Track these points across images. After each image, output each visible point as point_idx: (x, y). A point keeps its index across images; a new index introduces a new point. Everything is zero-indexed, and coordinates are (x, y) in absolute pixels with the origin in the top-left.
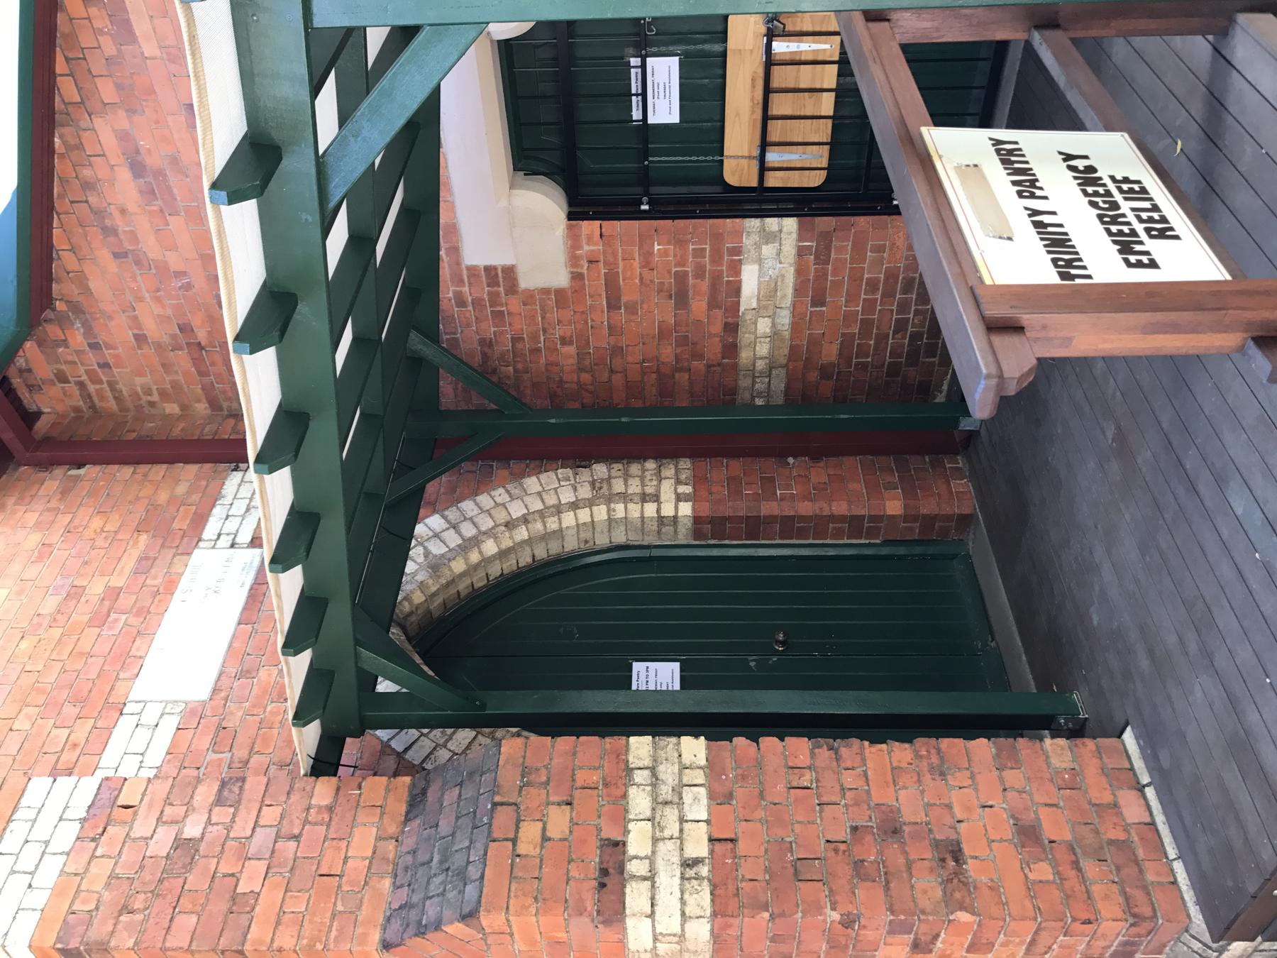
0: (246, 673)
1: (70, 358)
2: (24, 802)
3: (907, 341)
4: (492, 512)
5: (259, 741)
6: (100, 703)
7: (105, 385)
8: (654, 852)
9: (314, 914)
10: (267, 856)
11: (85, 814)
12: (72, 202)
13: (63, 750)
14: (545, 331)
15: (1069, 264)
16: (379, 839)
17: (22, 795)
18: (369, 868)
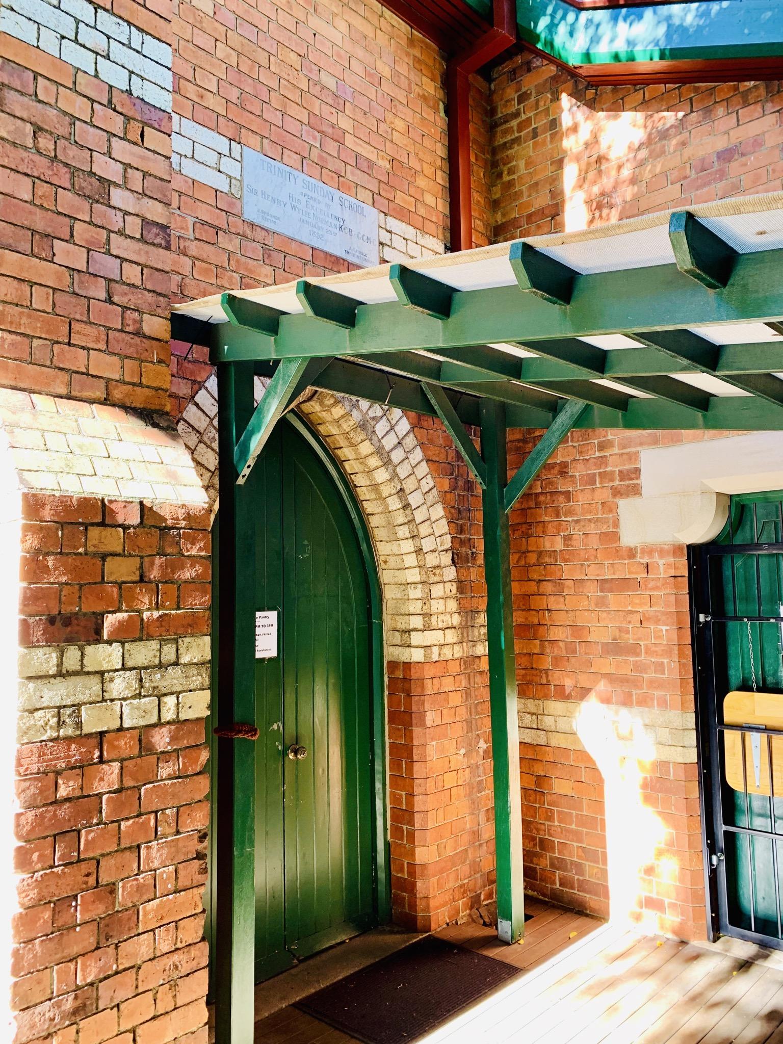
0: (267, 250)
1: (542, 103)
2: (148, 38)
3: (575, 859)
5: (205, 265)
6: (237, 124)
7: (517, 135)
8: (88, 673)
9: (29, 316)
10: (90, 270)
11: (135, 95)
12: (691, 99)
13: (197, 85)
14: (577, 521)
16: (108, 381)
17: (155, 37)
18: (77, 372)
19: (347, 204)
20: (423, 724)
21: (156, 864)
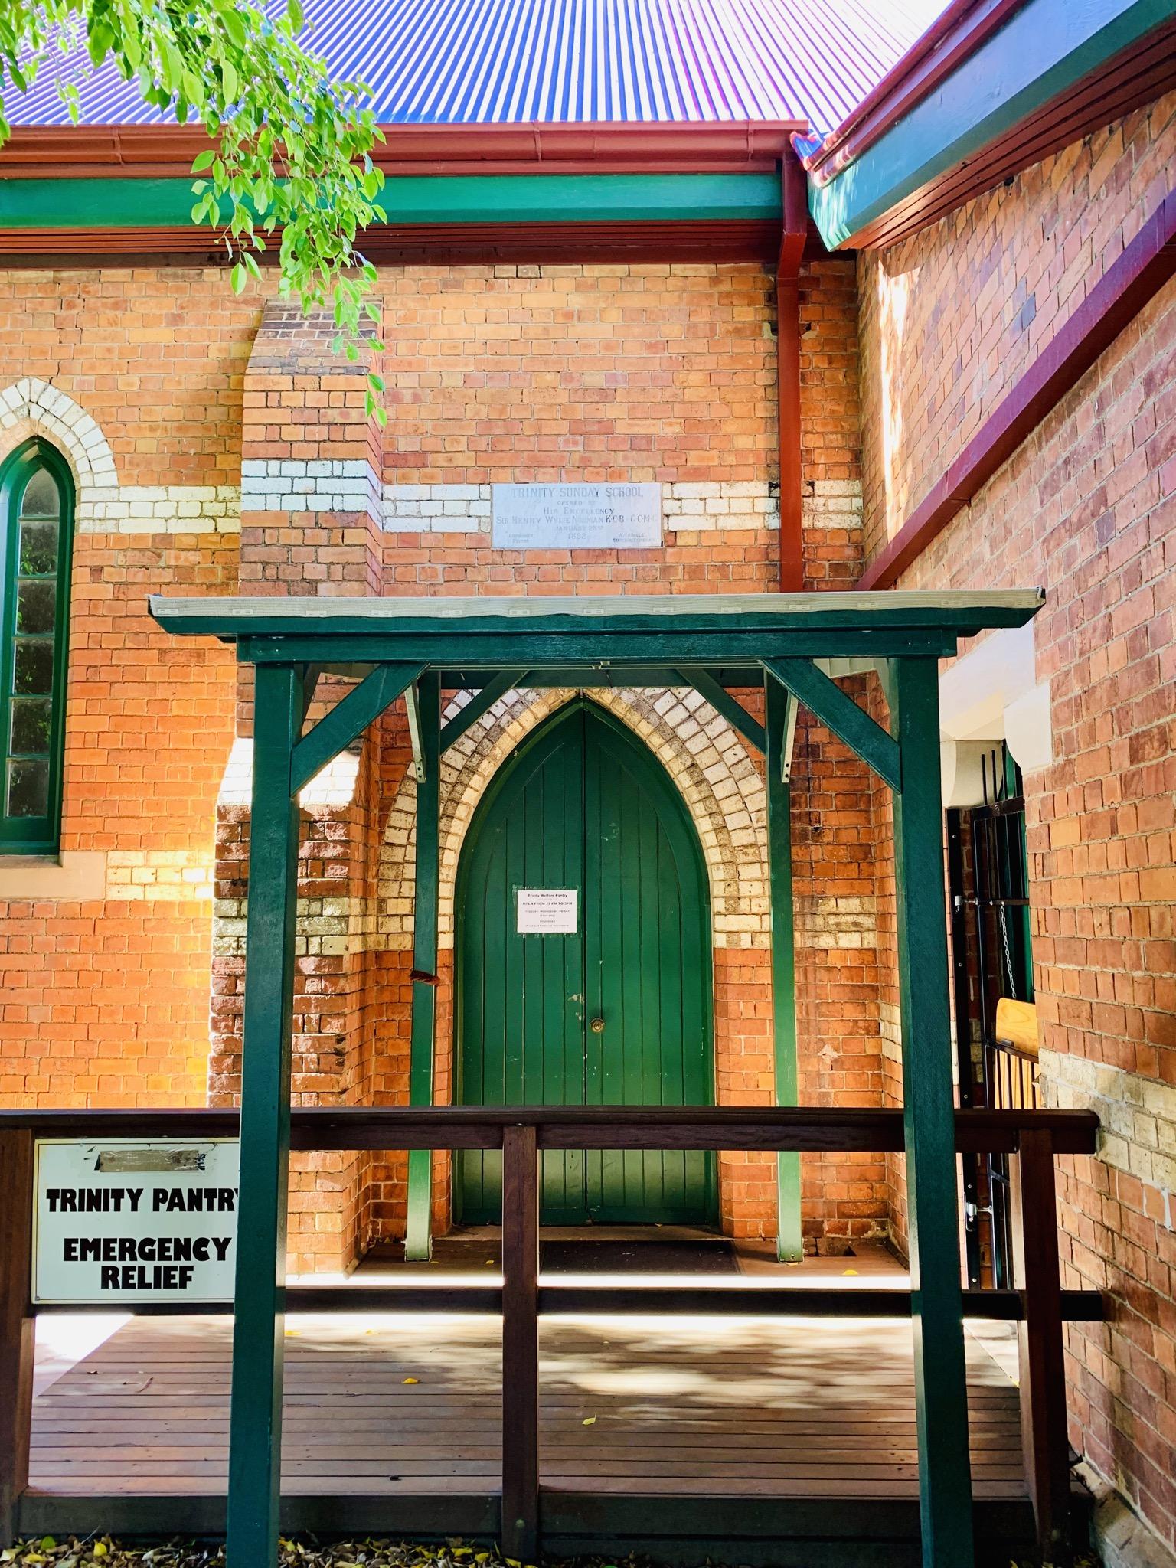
0: (519, 570)
4: (712, 749)
15: (72, 1201)
19: (617, 492)
20: (726, 1014)
21: (303, 1049)
